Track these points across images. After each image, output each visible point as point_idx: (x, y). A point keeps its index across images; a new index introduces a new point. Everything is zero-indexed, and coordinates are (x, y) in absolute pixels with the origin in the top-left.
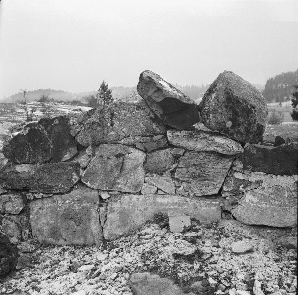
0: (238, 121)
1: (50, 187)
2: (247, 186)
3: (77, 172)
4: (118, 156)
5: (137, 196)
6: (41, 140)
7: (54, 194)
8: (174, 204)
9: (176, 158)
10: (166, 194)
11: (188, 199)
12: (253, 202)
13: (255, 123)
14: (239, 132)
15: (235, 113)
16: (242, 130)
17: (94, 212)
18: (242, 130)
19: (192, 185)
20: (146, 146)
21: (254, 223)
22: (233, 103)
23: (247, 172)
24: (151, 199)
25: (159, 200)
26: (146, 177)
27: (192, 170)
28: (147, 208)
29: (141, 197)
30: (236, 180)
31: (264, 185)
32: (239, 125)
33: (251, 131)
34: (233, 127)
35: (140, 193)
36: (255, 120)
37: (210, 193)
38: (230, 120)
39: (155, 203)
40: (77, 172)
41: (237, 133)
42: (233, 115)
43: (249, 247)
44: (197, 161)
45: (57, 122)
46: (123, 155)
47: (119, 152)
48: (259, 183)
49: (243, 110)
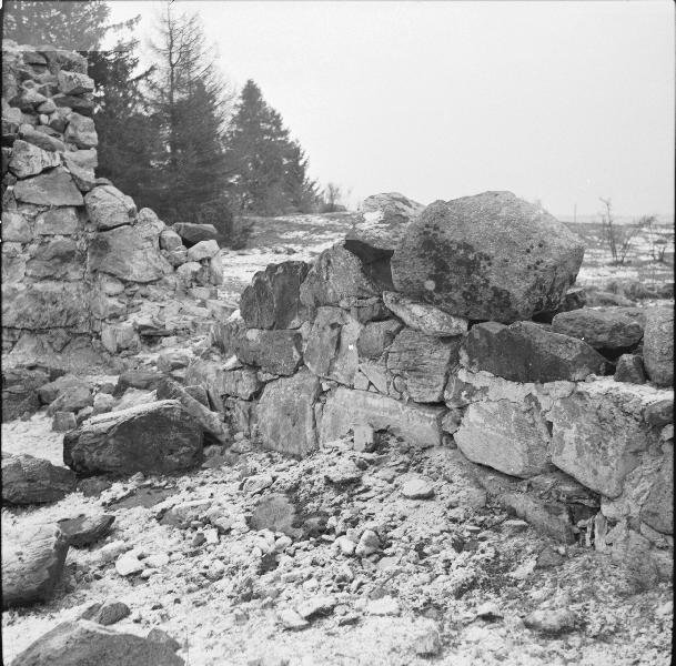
0: (448, 280)
1: (274, 365)
2: (473, 395)
3: (299, 347)
4: (333, 326)
5: (348, 391)
6: (266, 295)
7: (280, 376)
8: (384, 410)
9: (391, 336)
10: (378, 392)
11: (400, 405)
12: (478, 424)
13: (486, 286)
14: (449, 300)
15: (442, 266)
16: (456, 296)
17: (309, 408)
18: (456, 296)
19: (408, 382)
20: (615, 308)
21: (479, 461)
22: (438, 250)
23: (474, 369)
24: (362, 398)
25: (370, 400)
26: (360, 362)
27: (405, 356)
28: (357, 412)
29: (352, 393)
30: (459, 381)
31: (491, 394)
32: (449, 288)
33: (479, 299)
34: (438, 289)
35: (352, 388)
36: (488, 281)
37: (428, 400)
38: (431, 277)
39: (365, 405)
40: (299, 347)
41: (447, 300)
42: (437, 271)
43: (426, 491)
44: (411, 344)
45: (280, 270)
46: (339, 326)
47: (334, 321)
48: (485, 390)
49: (459, 262)
